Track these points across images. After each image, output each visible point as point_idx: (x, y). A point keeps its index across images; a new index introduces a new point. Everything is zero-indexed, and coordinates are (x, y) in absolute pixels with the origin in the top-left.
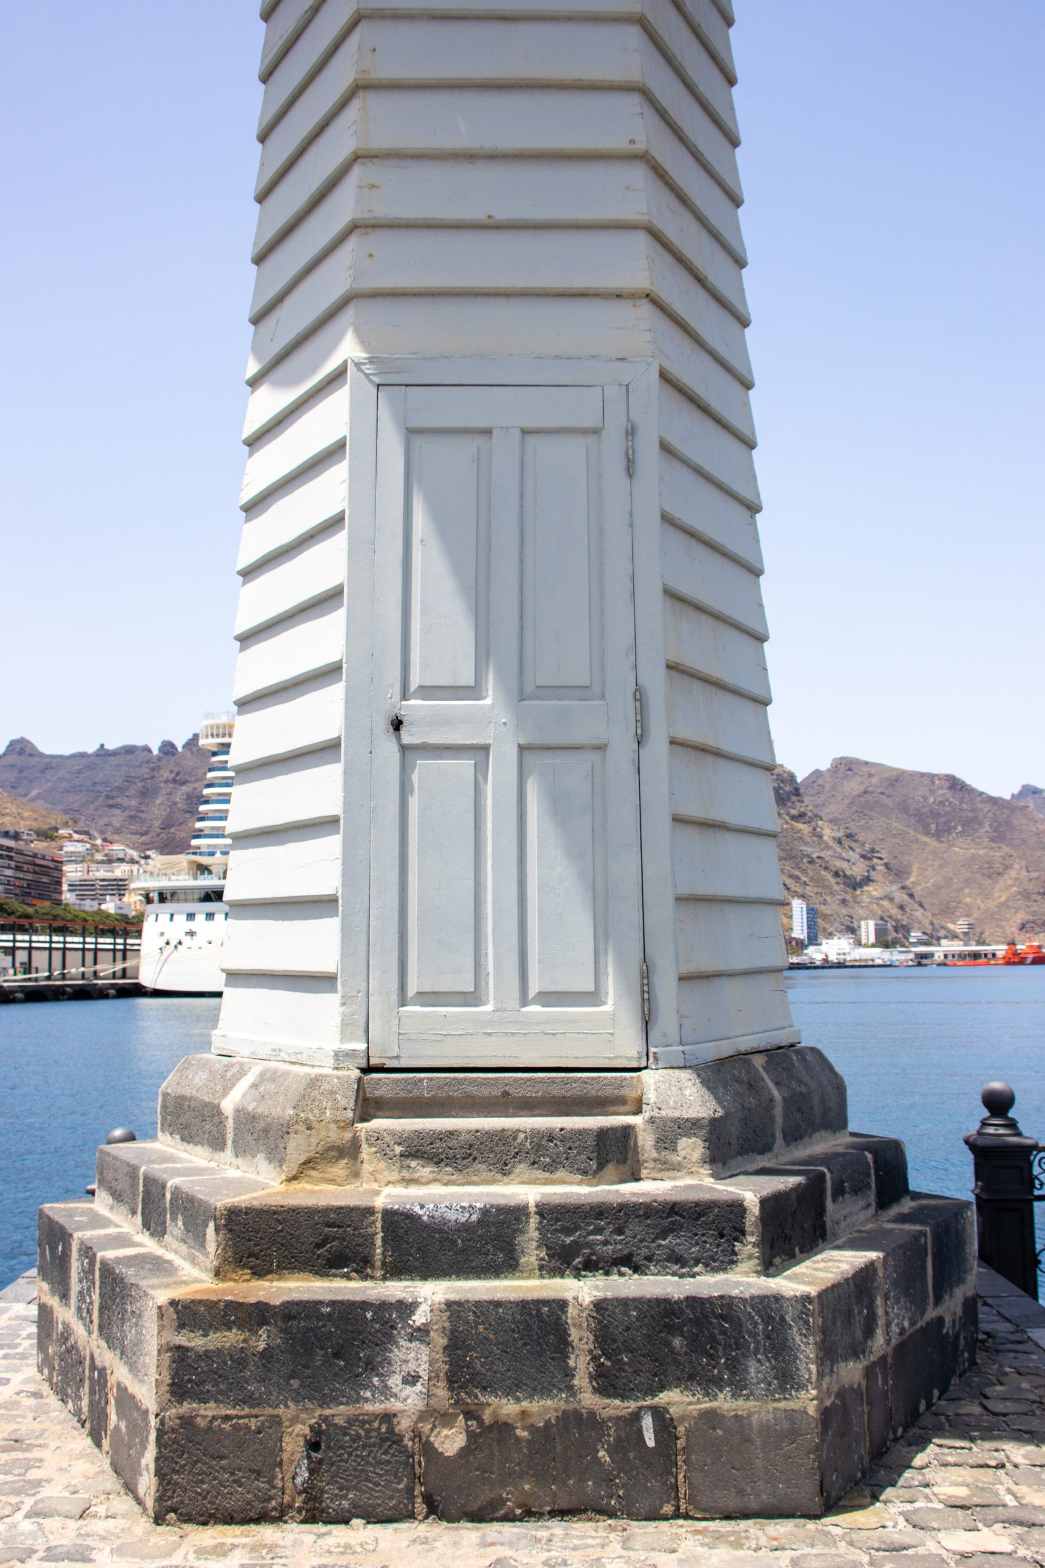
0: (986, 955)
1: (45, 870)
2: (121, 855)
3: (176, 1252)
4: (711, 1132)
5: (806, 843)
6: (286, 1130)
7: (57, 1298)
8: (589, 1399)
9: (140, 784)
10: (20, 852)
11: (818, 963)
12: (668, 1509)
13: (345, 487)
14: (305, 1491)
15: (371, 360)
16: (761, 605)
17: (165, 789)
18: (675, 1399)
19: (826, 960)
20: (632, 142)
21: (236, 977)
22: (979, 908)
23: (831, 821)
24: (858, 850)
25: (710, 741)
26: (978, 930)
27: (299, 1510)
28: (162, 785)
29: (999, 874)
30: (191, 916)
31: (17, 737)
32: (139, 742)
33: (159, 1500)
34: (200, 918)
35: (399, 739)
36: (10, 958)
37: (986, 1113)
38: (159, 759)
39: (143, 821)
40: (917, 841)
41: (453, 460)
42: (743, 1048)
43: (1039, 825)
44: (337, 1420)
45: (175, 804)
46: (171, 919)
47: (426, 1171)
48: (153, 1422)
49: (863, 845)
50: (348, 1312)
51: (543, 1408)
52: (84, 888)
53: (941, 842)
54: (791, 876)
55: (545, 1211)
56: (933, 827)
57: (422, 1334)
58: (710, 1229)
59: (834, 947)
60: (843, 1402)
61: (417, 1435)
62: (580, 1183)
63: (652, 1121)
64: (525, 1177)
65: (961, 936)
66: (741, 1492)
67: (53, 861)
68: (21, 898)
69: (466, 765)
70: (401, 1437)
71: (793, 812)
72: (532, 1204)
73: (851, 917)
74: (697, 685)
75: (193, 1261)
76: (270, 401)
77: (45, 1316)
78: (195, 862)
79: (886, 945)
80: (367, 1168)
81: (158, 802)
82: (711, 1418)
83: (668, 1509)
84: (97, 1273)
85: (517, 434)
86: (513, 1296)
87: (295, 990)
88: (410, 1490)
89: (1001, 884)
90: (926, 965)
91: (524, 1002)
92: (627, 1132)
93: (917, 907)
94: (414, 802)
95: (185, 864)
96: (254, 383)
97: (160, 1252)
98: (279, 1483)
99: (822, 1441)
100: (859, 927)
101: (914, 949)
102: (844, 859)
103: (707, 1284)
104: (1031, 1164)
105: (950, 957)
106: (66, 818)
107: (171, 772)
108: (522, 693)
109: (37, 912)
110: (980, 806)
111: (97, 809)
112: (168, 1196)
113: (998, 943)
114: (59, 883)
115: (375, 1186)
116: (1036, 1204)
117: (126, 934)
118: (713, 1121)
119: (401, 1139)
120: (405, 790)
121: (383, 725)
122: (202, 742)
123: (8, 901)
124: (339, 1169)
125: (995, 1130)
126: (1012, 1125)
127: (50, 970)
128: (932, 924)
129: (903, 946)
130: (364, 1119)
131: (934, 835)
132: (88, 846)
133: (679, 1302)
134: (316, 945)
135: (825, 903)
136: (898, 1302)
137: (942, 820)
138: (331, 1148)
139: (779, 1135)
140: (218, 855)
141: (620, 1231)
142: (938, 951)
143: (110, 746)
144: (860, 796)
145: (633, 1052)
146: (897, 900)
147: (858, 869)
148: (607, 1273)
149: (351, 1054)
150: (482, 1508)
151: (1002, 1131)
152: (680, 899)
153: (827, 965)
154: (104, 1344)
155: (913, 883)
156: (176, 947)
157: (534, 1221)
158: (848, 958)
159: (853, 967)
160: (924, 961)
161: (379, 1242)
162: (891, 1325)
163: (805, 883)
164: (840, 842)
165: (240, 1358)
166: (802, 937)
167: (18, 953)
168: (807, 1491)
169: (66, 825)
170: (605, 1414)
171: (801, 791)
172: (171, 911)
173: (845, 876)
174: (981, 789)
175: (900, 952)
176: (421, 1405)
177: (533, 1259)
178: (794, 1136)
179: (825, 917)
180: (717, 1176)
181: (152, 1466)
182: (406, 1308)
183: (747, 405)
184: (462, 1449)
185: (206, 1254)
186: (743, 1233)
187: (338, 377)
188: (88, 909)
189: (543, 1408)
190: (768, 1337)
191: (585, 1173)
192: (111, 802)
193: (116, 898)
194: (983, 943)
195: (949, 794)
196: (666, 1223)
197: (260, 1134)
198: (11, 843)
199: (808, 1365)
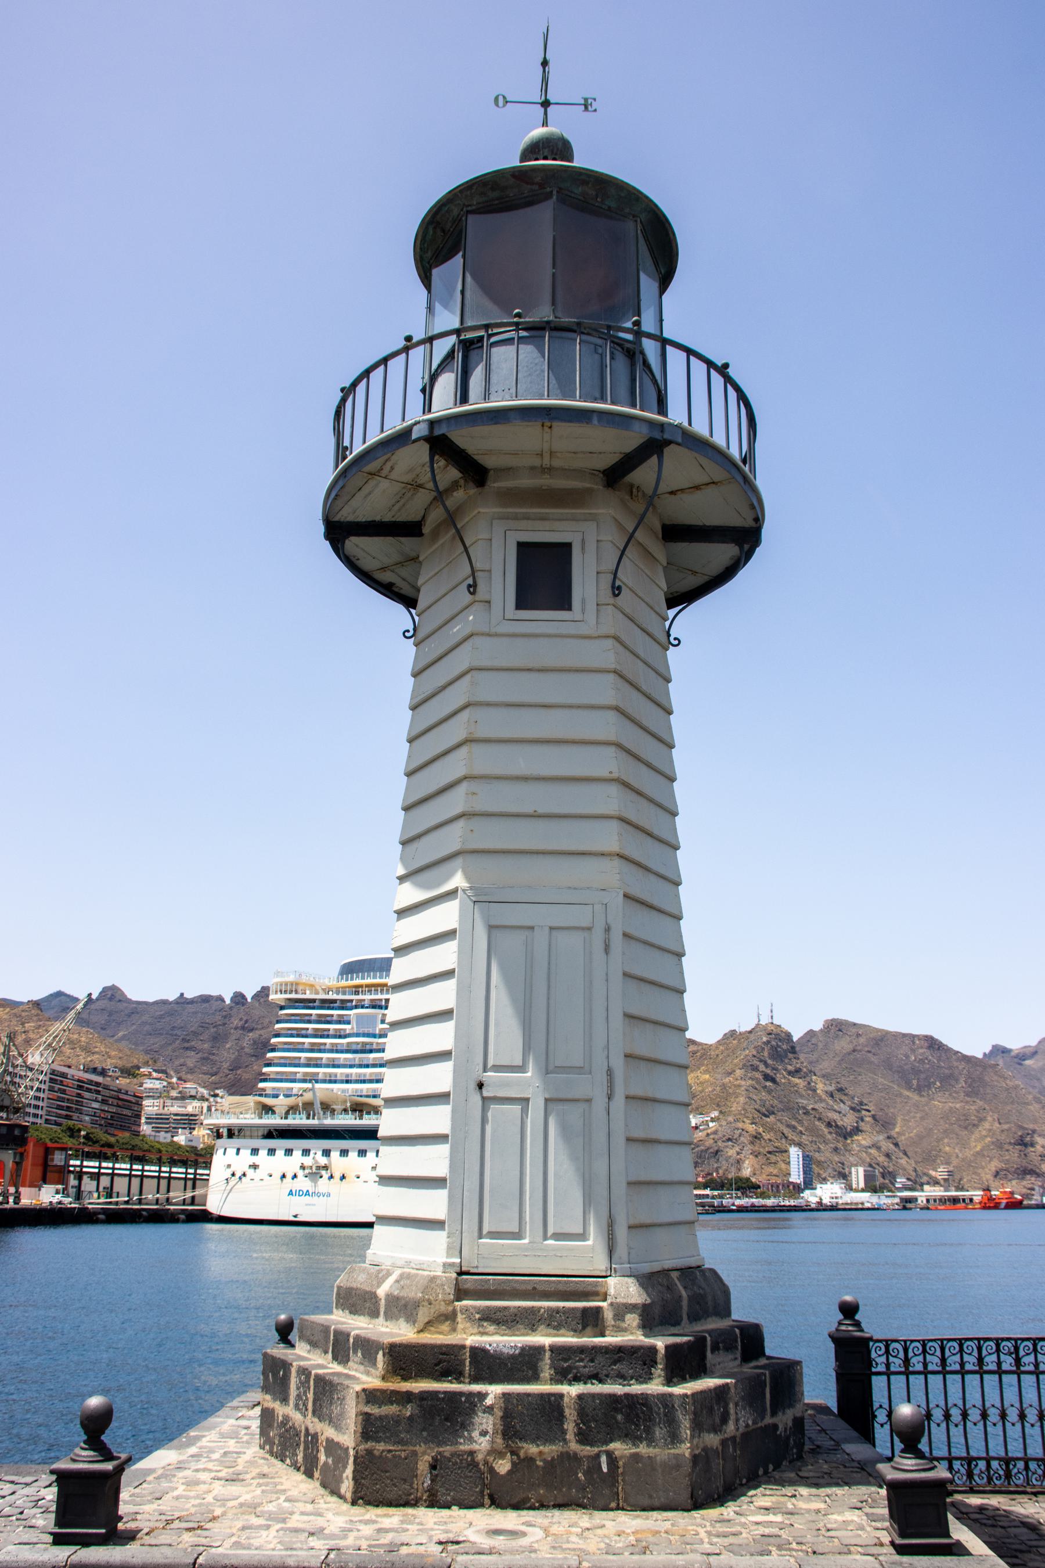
0: (964, 1200)
1: (126, 1104)
2: (193, 1093)
3: (356, 1370)
4: (643, 1311)
5: (802, 1096)
6: (417, 1304)
7: (278, 1403)
8: (574, 1446)
9: (213, 1030)
10: (106, 1087)
11: (813, 1206)
12: (613, 1505)
13: (456, 955)
14: (429, 1491)
15: (471, 888)
16: (684, 1011)
17: (235, 1034)
18: (618, 1447)
19: (820, 1203)
20: (611, 772)
21: (379, 1218)
22: (957, 1156)
23: (823, 1076)
24: (849, 1103)
25: (650, 1095)
26: (957, 1177)
27: (425, 1501)
28: (232, 1031)
29: (974, 1125)
30: (255, 1151)
31: (109, 984)
32: (214, 992)
33: (354, 1492)
34: (263, 1153)
35: (481, 1094)
36: (95, 1183)
37: (841, 1317)
38: (231, 1008)
39: (214, 1063)
40: (901, 1095)
41: (513, 942)
42: (666, 1267)
43: (1008, 1082)
44: (445, 1454)
45: (243, 1048)
46: (238, 1153)
47: (492, 1328)
48: (352, 1452)
49: (853, 1098)
50: (452, 1397)
51: (550, 1450)
52: (160, 1121)
53: (921, 1096)
54: (788, 1126)
55: (553, 1349)
56: (915, 1082)
57: (490, 1410)
58: (639, 1360)
59: (828, 1192)
60: (706, 1454)
61: (486, 1463)
62: (573, 1336)
63: (612, 1304)
64: (544, 1333)
65: (942, 1182)
66: (651, 1497)
67: (135, 1096)
68: (105, 1129)
69: (517, 1108)
70: (478, 1464)
71: (790, 1068)
72: (547, 1345)
73: (843, 1164)
74: (643, 1064)
75: (368, 1373)
76: (410, 894)
77: (267, 1416)
78: (260, 1103)
79: (874, 1190)
80: (460, 1326)
81: (228, 1046)
82: (636, 1457)
83: (613, 1505)
84: (312, 1382)
85: (547, 929)
86: (536, 1392)
87: (419, 1228)
88: (482, 1492)
89: (976, 1135)
90: (910, 1209)
91: (545, 1238)
92: (598, 1310)
93: (901, 1155)
94: (489, 1128)
95: (252, 1104)
96: (402, 879)
97: (346, 1371)
98: (415, 1486)
99: (693, 1471)
100: (850, 1173)
101: (899, 1194)
102: (835, 1111)
103: (636, 1388)
104: (869, 1352)
105: (932, 1202)
106: (147, 1057)
107: (241, 1019)
108: (548, 1070)
109: (118, 1141)
110: (955, 1064)
111: (174, 1051)
112: (351, 1340)
113: (975, 1189)
114: (139, 1116)
115: (465, 1336)
116: (874, 1378)
117: (196, 1165)
118: (644, 1305)
119: (479, 1310)
120: (484, 1121)
121: (473, 1086)
122: (272, 997)
123: (93, 1130)
124: (445, 1327)
125: (848, 1328)
126: (857, 1324)
127: (129, 1195)
128: (915, 1170)
129: (889, 1191)
130: (459, 1299)
131: (915, 1090)
132: (165, 1084)
133: (621, 1396)
134: (433, 1204)
135: (819, 1150)
136: (745, 1409)
137: (923, 1076)
138: (441, 1315)
139: (685, 1316)
140: (281, 1097)
141: (592, 1361)
142: (921, 1197)
143: (189, 995)
144: (849, 1054)
145: (603, 1268)
146: (884, 1148)
147: (848, 1121)
148: (585, 1383)
149: (452, 1265)
150: (519, 1502)
151: (850, 1328)
152: (629, 1183)
153: (821, 1207)
154: (316, 1420)
155: (898, 1133)
156: (240, 1178)
157: (548, 1354)
158: (840, 1201)
159: (845, 1209)
160: (908, 1205)
161: (467, 1364)
162: (739, 1421)
163: (801, 1132)
164: (832, 1096)
165: (397, 1420)
166: (798, 1181)
167: (102, 1178)
168: (684, 1496)
169: (146, 1064)
170: (582, 1454)
171: (797, 1049)
172: (238, 1146)
173: (837, 1126)
174: (956, 1048)
175: (887, 1196)
176: (488, 1447)
177: (547, 1374)
178: (694, 1318)
179: (819, 1163)
180: (646, 1335)
181: (351, 1476)
182: (482, 1396)
183: (677, 896)
184: (509, 1471)
185: (377, 1369)
186: (656, 1363)
187: (452, 894)
188: (162, 1140)
189: (550, 1450)
190: (665, 1415)
191: (575, 1331)
192: (186, 1045)
193: (187, 1131)
194: (962, 1189)
195: (928, 1053)
196: (616, 1357)
197: (400, 1307)
198: (99, 1079)
199: (686, 1432)
